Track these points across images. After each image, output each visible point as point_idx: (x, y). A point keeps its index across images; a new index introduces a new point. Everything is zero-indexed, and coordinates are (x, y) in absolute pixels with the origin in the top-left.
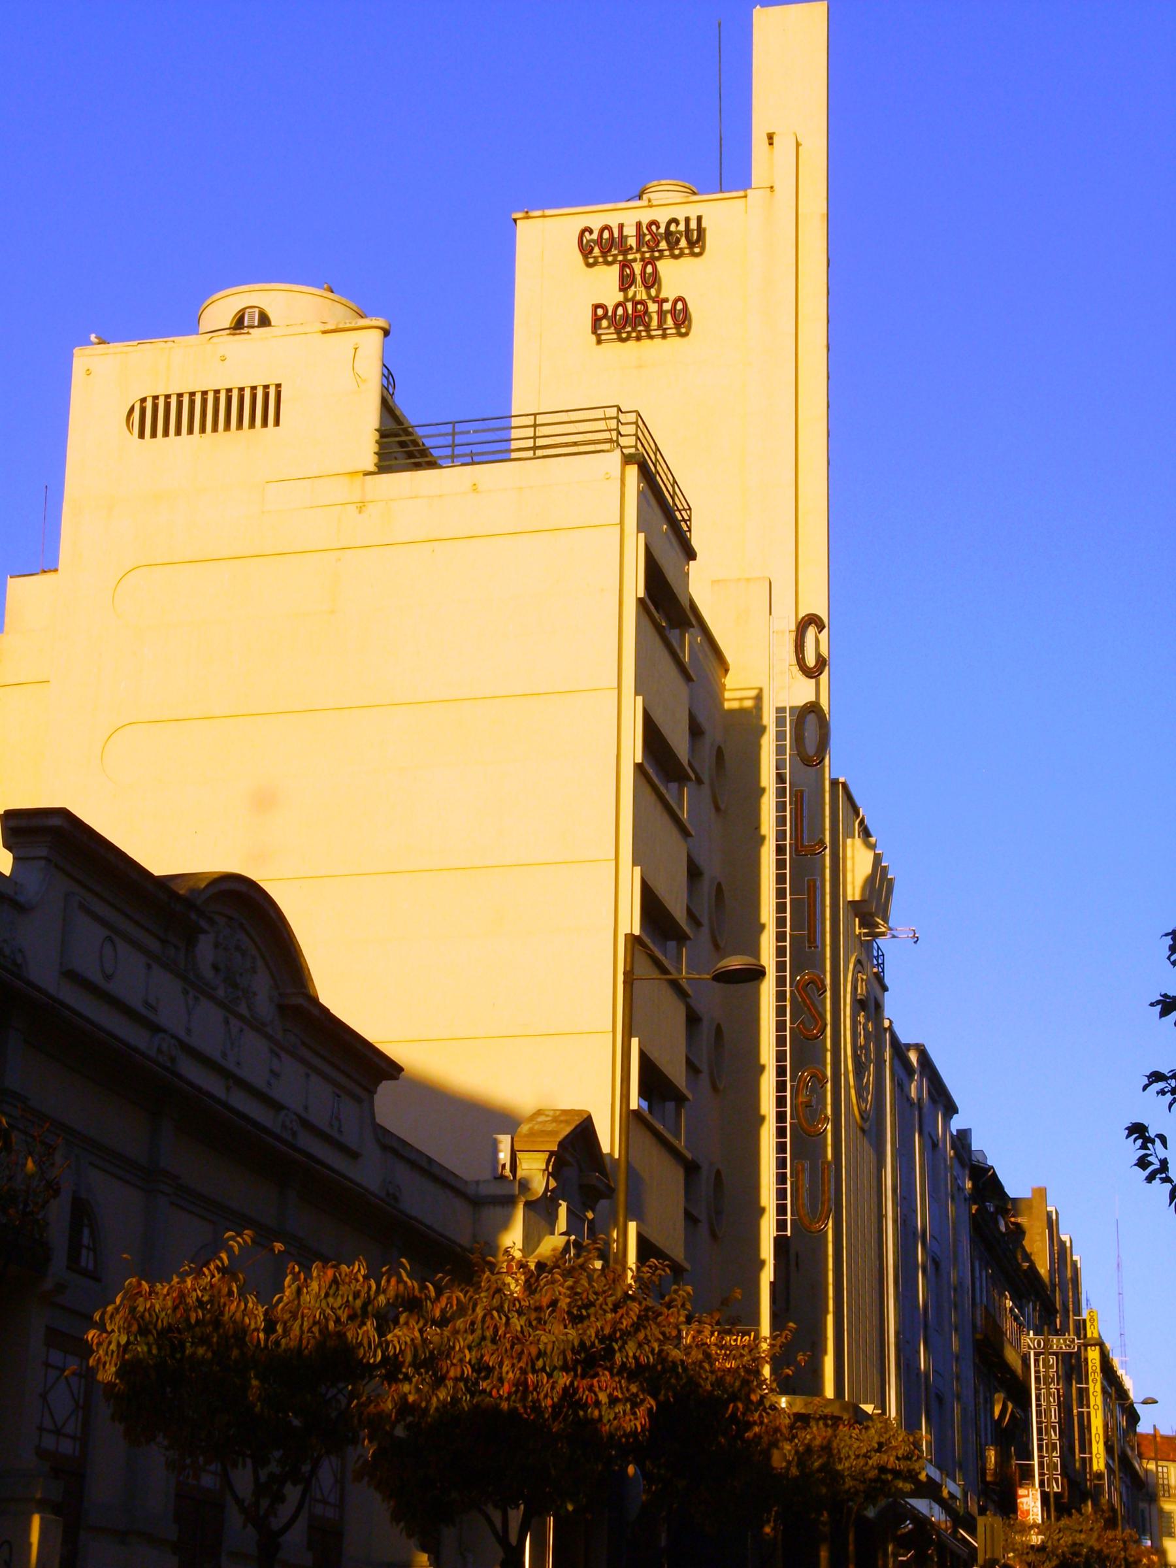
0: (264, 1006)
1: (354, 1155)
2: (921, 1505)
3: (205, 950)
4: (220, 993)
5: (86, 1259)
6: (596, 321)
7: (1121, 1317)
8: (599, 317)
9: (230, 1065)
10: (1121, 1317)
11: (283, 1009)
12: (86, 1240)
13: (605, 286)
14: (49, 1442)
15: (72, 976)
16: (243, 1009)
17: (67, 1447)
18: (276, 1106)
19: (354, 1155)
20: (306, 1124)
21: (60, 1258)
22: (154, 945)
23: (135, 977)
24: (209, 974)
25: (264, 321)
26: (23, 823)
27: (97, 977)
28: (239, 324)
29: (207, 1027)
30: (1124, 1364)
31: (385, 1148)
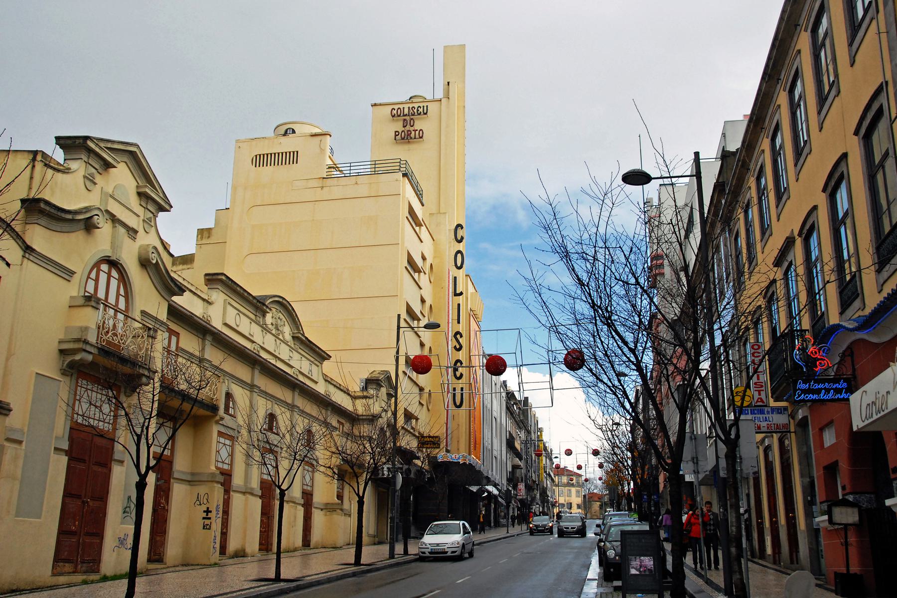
0: (288, 337)
1: (316, 383)
2: (490, 488)
3: (269, 318)
4: (274, 332)
5: (231, 411)
6: (396, 135)
7: (199, 297)
8: (397, 133)
9: (276, 354)
10: (199, 297)
11: (294, 338)
12: (231, 405)
13: (399, 126)
14: (220, 465)
15: (226, 325)
16: (281, 337)
17: (226, 467)
18: (292, 367)
19: (316, 383)
20: (301, 372)
21: (221, 412)
22: (253, 317)
23: (246, 325)
24: (270, 326)
25: (294, 132)
26: (210, 277)
27: (235, 327)
28: (286, 134)
29: (269, 342)
30: (27, 507)
31: (326, 381)
